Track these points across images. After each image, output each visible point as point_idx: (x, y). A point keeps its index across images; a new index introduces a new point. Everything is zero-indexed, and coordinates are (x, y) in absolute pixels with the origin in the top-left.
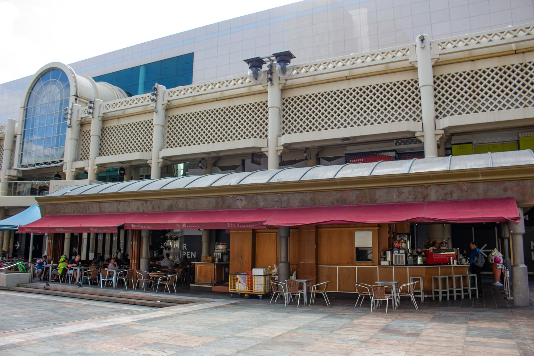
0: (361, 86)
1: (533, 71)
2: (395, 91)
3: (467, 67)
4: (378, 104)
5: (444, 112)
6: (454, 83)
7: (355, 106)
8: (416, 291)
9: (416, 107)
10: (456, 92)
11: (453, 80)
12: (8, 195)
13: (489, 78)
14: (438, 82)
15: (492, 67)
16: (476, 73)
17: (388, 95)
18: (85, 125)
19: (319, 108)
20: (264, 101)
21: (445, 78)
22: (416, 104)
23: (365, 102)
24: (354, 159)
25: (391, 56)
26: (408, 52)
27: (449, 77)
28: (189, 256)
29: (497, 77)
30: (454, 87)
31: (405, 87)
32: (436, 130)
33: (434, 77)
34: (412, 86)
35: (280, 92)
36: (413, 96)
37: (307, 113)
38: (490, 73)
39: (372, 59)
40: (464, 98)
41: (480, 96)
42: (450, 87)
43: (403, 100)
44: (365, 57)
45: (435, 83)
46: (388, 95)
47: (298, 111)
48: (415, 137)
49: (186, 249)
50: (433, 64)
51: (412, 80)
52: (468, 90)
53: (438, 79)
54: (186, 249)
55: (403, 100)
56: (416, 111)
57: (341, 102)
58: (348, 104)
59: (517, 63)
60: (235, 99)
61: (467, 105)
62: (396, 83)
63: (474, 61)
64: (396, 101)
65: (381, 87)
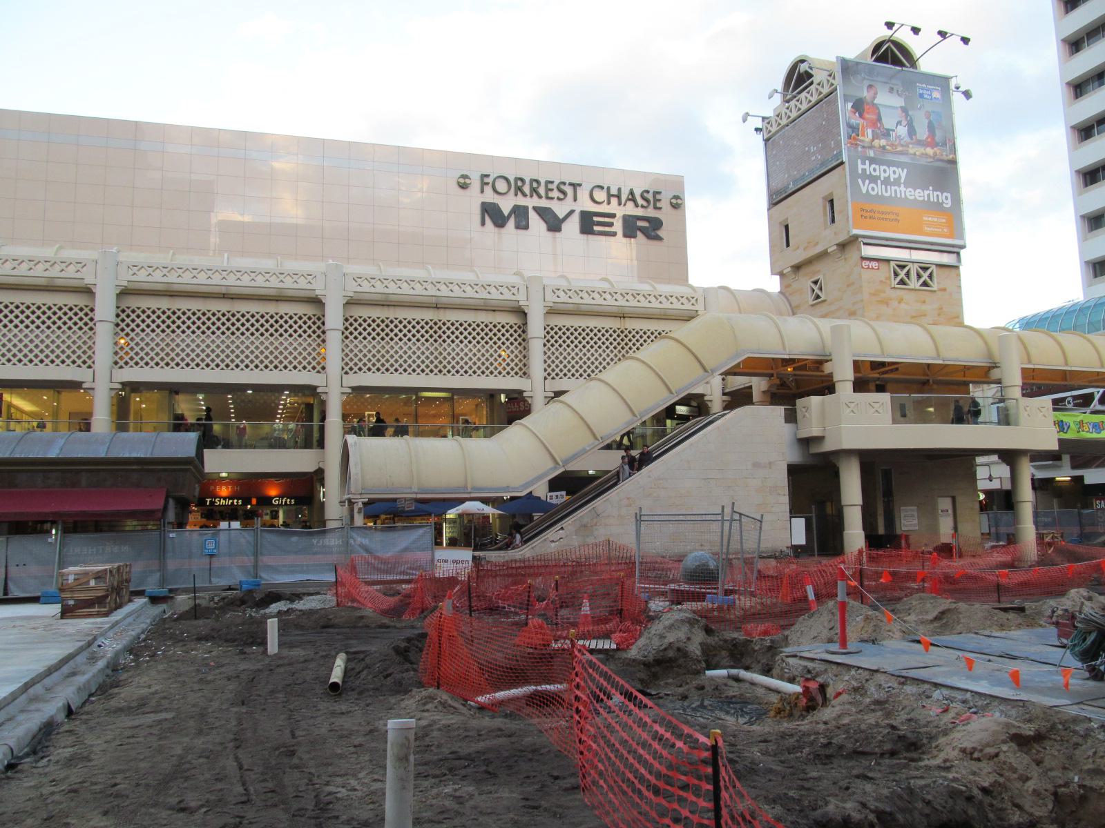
0: (584, 326)
2: (70, 319)
3: (428, 315)
4: (495, 335)
6: (60, 318)
9: (61, 330)
10: (206, 326)
11: (28, 312)
13: (33, 317)
14: (123, 316)
15: (427, 319)
16: (392, 322)
20: (319, 314)
21: (133, 312)
25: (207, 276)
26: (85, 268)
27: (139, 312)
29: (76, 319)
30: (22, 317)
31: (76, 314)
33: (118, 307)
34: (86, 315)
35: (115, 297)
36: (576, 334)
38: (161, 315)
39: (29, 268)
40: (250, 332)
41: (161, 329)
42: (17, 317)
43: (491, 334)
44: (182, 270)
45: (118, 316)
47: (400, 331)
50: (118, 292)
51: (228, 312)
52: (141, 323)
53: (123, 311)
55: (572, 338)
56: (145, 337)
58: (383, 330)
59: (224, 310)
60: (397, 308)
61: (80, 336)
62: (52, 306)
64: (482, 334)
65: (50, 308)
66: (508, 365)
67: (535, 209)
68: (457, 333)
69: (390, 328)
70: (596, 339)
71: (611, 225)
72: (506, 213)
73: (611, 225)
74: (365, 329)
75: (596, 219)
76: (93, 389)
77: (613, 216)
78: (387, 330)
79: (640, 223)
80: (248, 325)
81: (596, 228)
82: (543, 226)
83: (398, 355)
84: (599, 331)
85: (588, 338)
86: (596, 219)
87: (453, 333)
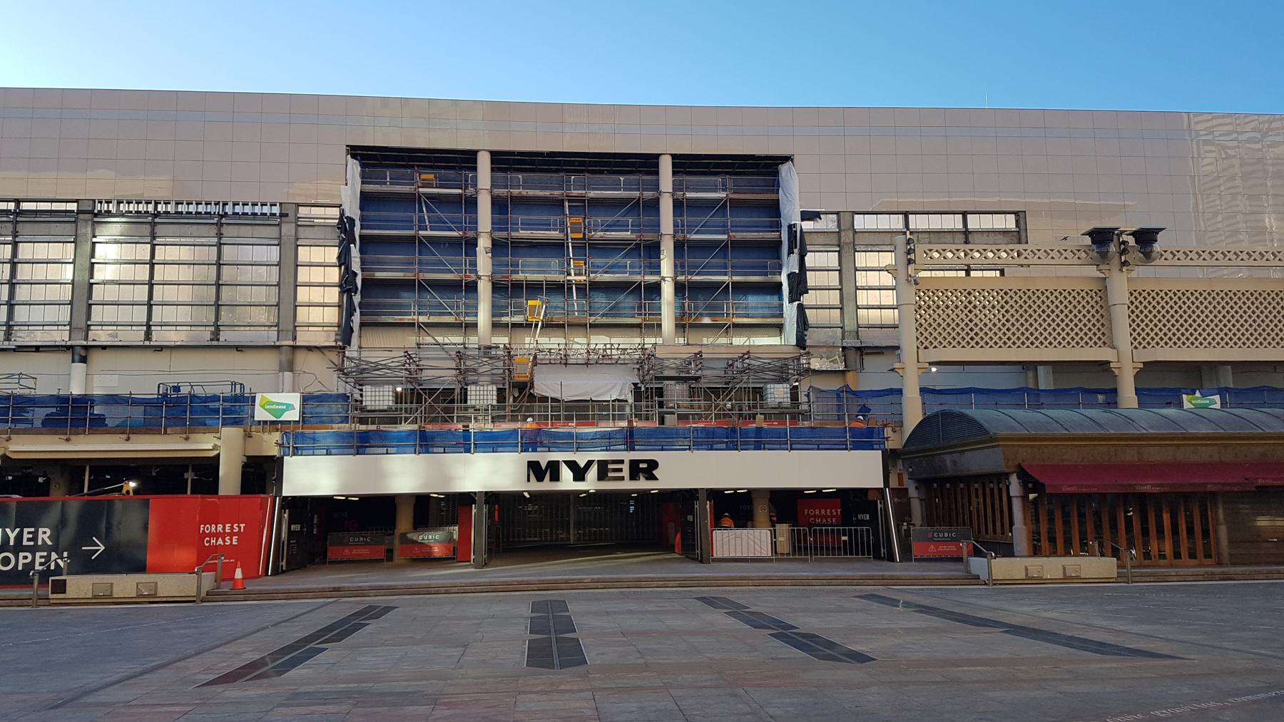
1: (1282, 323)
5: (935, 343)
7: (1059, 330)
8: (409, 412)
12: (361, 192)
17: (1195, 325)
18: (320, 353)
19: (1247, 326)
22: (1216, 341)
23: (1143, 325)
24: (1260, 693)
28: (29, 540)
32: (918, 362)
37: (1191, 326)
43: (1183, 330)
46: (1195, 325)
47: (1186, 321)
48: (87, 170)
49: (49, 543)
54: (49, 543)
55: (1204, 325)
57: (1181, 321)
58: (1076, 325)
63: (107, 349)
66: (1021, 307)
67: (565, 462)
68: (1063, 334)
69: (1223, 323)
70: (1204, 325)
71: (621, 470)
72: (544, 467)
73: (621, 470)
74: (1062, 321)
75: (610, 466)
76: (898, 348)
77: (622, 462)
78: (1027, 334)
79: (642, 466)
80: (1081, 325)
81: (610, 474)
82: (571, 475)
83: (968, 309)
84: (1078, 343)
85: (1205, 334)
86: (610, 466)
87: (1237, 321)
